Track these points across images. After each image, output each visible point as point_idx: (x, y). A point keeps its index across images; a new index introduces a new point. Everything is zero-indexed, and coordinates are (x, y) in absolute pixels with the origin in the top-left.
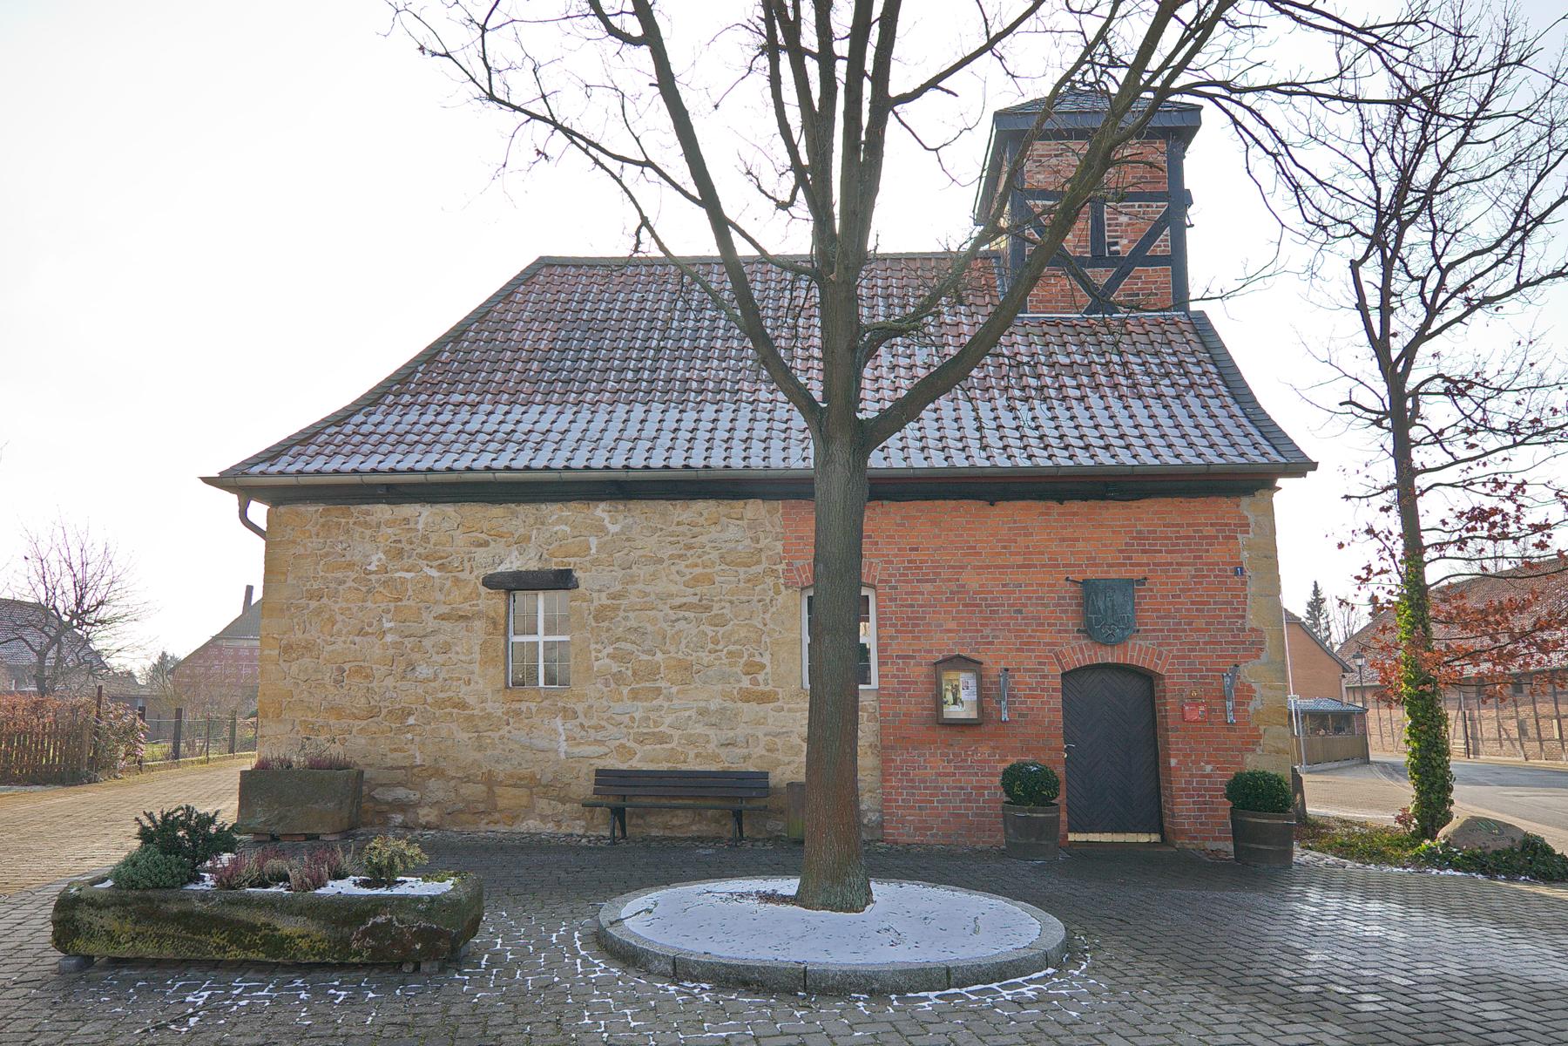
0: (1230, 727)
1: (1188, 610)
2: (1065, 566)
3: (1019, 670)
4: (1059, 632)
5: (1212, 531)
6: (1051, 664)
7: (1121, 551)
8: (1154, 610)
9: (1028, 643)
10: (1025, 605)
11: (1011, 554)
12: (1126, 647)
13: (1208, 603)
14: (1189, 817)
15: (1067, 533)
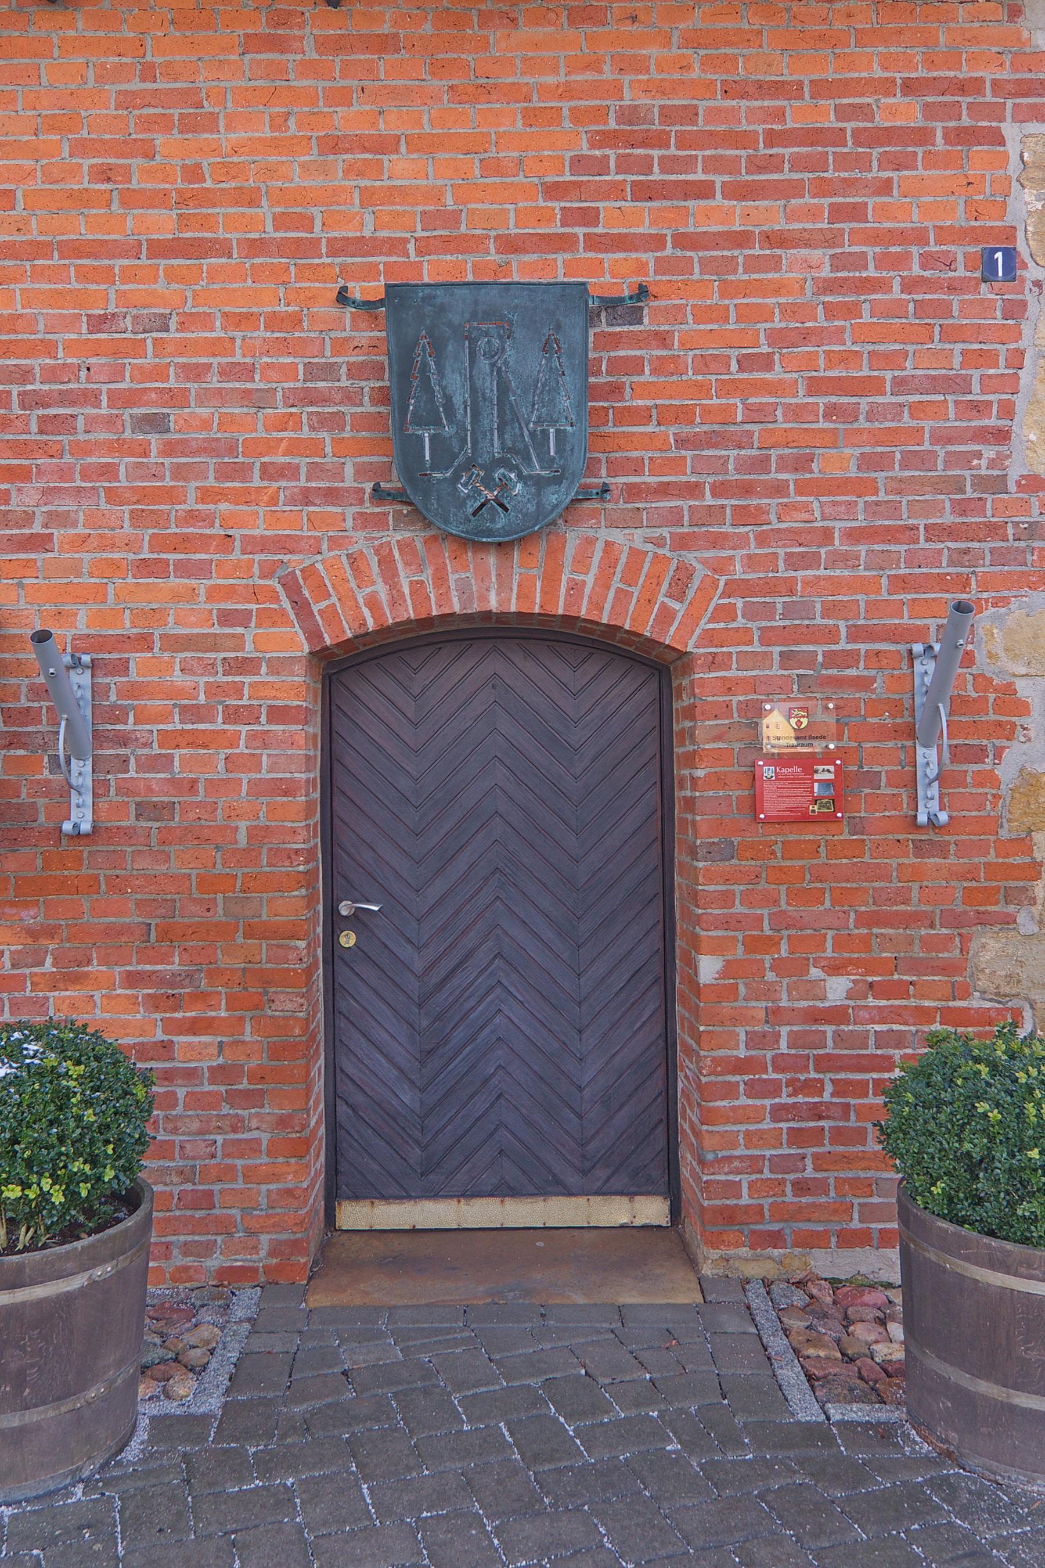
0: (928, 839)
1: (796, 412)
2: (338, 247)
3: (144, 642)
4: (306, 497)
5: (904, 111)
6: (276, 618)
7: (553, 191)
8: (666, 416)
9: (183, 543)
10: (177, 398)
11: (130, 199)
12: (555, 553)
13: (874, 386)
14: (754, 1164)
15: (344, 119)
